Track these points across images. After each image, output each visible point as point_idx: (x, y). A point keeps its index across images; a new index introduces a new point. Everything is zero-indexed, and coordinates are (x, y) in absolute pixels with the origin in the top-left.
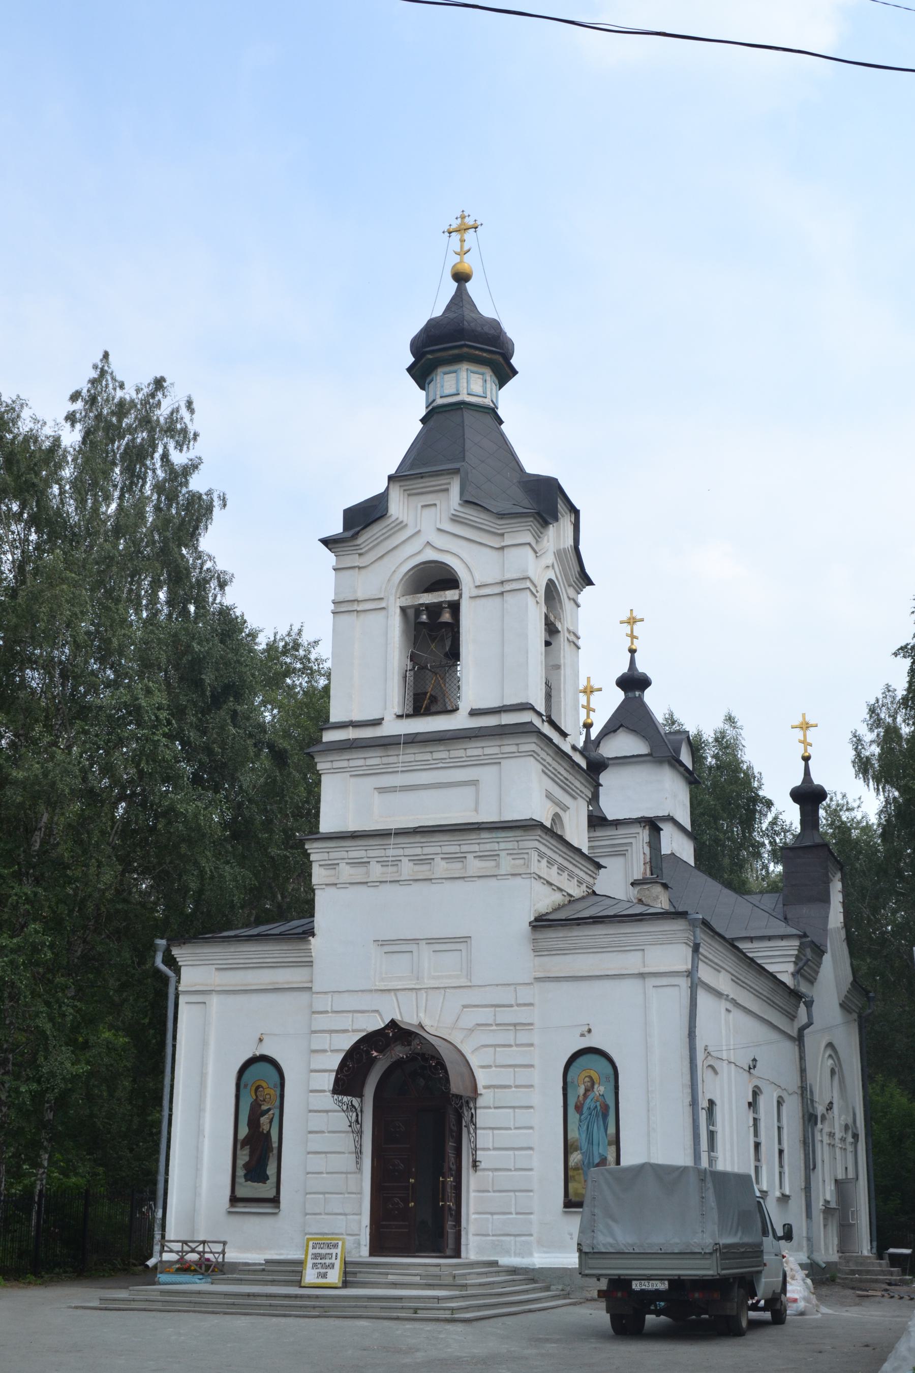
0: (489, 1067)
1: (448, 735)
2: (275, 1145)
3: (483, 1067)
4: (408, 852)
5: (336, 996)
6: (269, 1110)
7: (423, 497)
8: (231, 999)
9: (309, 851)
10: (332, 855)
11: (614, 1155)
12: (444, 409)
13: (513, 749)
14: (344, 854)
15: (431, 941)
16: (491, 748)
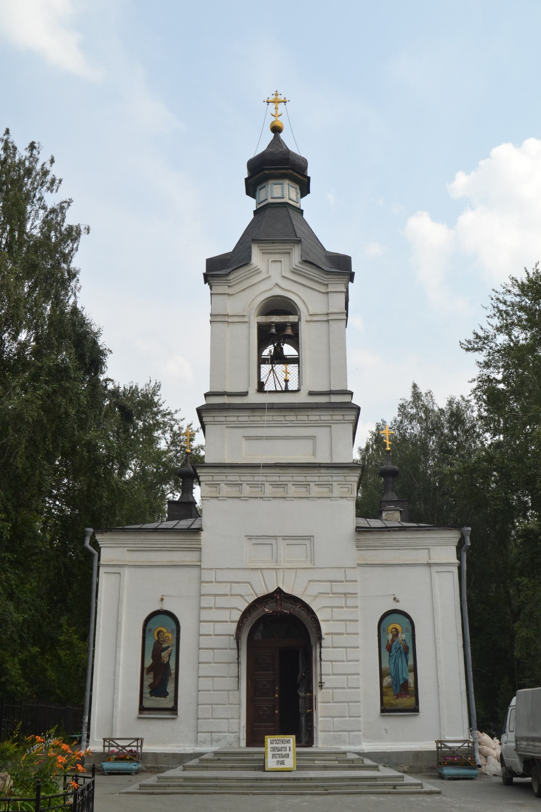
0: (328, 621)
1: (296, 406)
2: (173, 671)
3: (324, 621)
4: (269, 479)
5: (218, 571)
6: (168, 647)
7: (271, 256)
8: (139, 571)
9: (199, 474)
10: (215, 478)
11: (413, 678)
12: (276, 206)
13: (341, 418)
14: (224, 478)
15: (285, 538)
16: (326, 416)
